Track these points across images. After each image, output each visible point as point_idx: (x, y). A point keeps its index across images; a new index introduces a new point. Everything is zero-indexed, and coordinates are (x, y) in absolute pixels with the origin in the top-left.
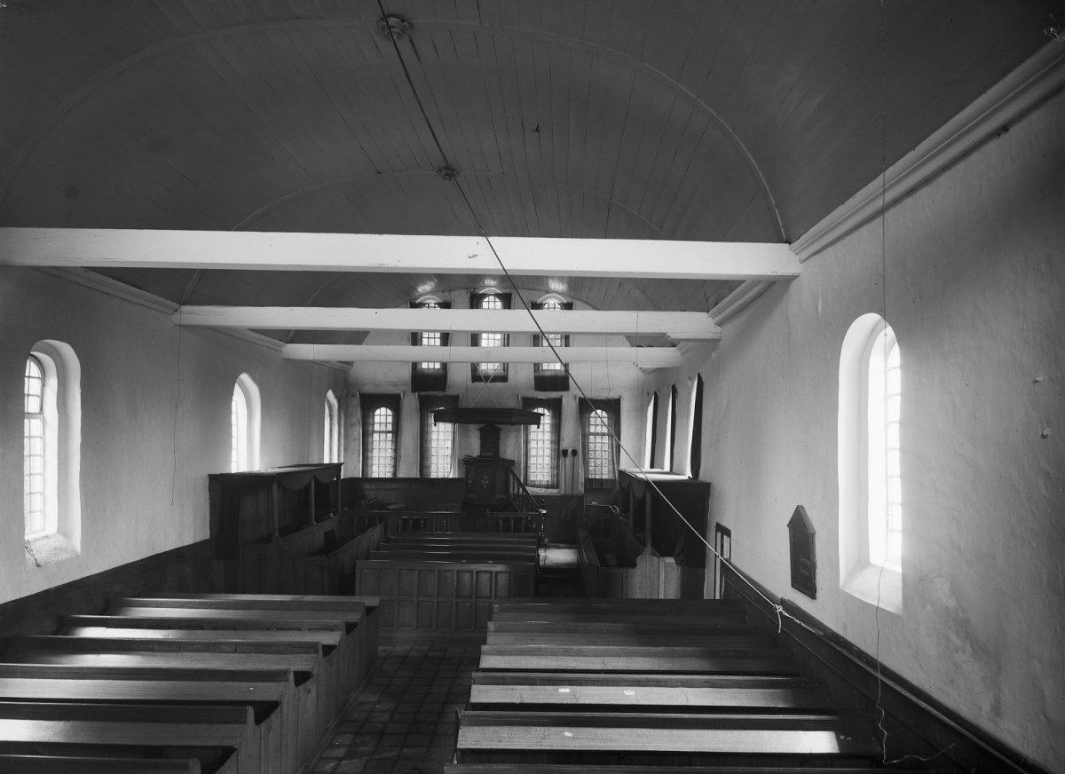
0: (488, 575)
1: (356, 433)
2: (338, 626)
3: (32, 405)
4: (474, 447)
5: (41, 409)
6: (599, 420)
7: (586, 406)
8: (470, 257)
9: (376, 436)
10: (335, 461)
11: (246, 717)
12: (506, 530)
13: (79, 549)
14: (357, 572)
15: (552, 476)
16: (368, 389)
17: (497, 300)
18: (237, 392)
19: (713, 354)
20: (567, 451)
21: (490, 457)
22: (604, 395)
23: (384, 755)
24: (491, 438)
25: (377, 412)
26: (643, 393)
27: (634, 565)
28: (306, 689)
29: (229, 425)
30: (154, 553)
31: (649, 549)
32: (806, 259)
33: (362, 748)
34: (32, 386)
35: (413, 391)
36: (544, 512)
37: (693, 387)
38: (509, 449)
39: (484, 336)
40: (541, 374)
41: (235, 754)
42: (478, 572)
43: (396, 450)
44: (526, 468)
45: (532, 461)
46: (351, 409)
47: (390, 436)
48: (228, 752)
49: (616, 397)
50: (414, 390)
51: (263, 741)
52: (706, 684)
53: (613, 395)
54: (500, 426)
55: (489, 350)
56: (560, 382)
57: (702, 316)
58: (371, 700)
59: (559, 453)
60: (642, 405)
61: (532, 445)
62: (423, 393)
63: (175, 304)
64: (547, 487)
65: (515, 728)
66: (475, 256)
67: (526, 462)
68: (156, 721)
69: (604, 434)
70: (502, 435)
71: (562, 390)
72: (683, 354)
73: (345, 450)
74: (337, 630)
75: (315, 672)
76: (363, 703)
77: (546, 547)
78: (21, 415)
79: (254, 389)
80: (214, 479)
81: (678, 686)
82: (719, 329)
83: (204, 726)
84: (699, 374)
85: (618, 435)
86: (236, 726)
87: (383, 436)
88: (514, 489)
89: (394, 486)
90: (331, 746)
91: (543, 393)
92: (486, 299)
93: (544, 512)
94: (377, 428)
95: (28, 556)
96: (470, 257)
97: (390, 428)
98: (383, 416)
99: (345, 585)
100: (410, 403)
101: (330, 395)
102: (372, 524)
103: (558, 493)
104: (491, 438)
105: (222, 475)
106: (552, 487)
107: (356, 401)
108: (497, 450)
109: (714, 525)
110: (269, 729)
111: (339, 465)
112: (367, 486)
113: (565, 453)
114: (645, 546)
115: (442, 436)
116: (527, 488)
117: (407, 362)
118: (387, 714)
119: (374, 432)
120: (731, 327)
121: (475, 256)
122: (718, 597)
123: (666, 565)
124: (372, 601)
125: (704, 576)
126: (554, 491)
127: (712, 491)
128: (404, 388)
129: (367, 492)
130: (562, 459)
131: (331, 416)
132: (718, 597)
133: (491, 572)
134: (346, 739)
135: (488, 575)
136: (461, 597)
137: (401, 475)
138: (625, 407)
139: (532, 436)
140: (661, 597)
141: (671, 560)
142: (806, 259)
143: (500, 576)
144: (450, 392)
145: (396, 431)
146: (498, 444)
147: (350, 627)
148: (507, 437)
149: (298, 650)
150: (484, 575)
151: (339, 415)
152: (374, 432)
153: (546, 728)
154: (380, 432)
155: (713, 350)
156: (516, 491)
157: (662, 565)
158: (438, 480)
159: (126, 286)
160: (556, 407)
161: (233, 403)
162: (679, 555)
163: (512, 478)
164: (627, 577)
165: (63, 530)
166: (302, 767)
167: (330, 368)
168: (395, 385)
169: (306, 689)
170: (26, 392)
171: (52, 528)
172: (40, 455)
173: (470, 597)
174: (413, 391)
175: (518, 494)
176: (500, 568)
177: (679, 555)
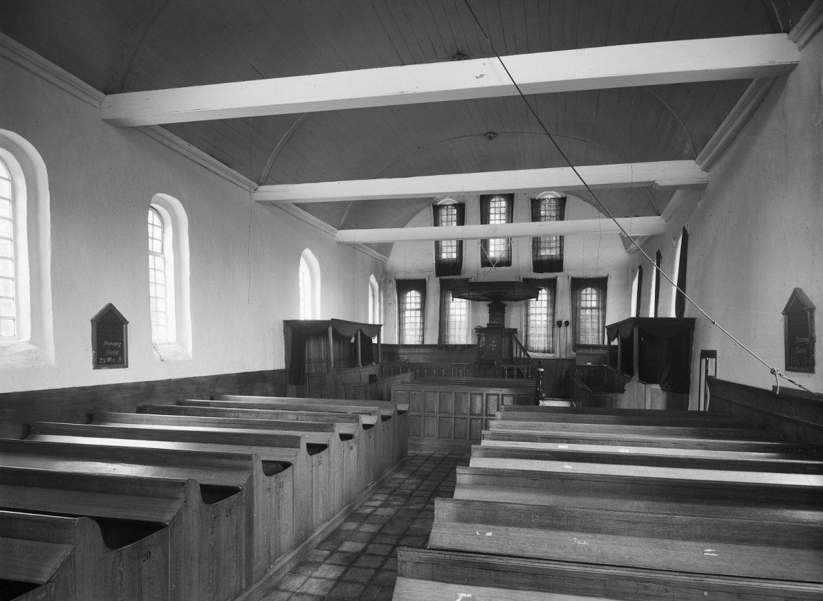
0: (496, 397)
1: (392, 311)
2: (375, 411)
3: (154, 246)
4: (484, 319)
5: (162, 251)
6: (590, 297)
7: (578, 284)
8: (477, 77)
9: (407, 314)
10: (377, 323)
11: (299, 443)
12: (511, 376)
13: (191, 355)
14: (393, 393)
15: (548, 343)
16: (401, 276)
17: (502, 199)
18: (302, 260)
19: (699, 204)
20: (561, 322)
21: (497, 325)
22: (592, 275)
23: (412, 507)
24: (497, 310)
25: (408, 294)
26: (628, 270)
27: (622, 391)
28: (349, 444)
29: (298, 288)
30: (244, 371)
31: (636, 377)
32: (806, 43)
33: (395, 503)
34: (154, 231)
35: (437, 277)
36: (542, 370)
37: (677, 245)
38: (513, 319)
39: (492, 241)
40: (539, 258)
41: (291, 467)
42: (487, 395)
43: (423, 323)
44: (527, 336)
45: (531, 331)
46: (388, 291)
47: (419, 312)
48: (286, 465)
49: (604, 275)
50: (437, 275)
51: (314, 468)
52: (698, 446)
53: (601, 274)
54: (505, 302)
55: (496, 227)
56: (556, 265)
57: (690, 164)
58: (402, 477)
59: (556, 324)
60: (628, 282)
61: (532, 318)
62: (444, 277)
63: (253, 183)
64: (544, 352)
65: (520, 460)
66: (482, 76)
67: (527, 331)
68: (234, 444)
69: (592, 308)
70: (507, 309)
71: (558, 272)
72: (666, 221)
73: (385, 313)
74: (374, 414)
75: (356, 435)
76: (395, 479)
77: (543, 399)
78: (145, 252)
79: (315, 263)
80: (287, 323)
81: (671, 448)
82: (705, 174)
83: (269, 448)
84: (684, 228)
85: (604, 308)
86: (293, 449)
87: (413, 313)
88: (517, 353)
89: (422, 351)
90: (370, 500)
91: (541, 274)
92: (494, 200)
93: (542, 370)
94: (408, 306)
95: (154, 352)
96: (477, 77)
97: (418, 306)
98: (413, 297)
99: (381, 396)
100: (434, 286)
101: (373, 279)
102: (405, 371)
103: (554, 356)
104: (497, 310)
105: (292, 321)
106: (549, 352)
107: (393, 286)
108: (503, 321)
109: (699, 353)
110: (320, 463)
111: (380, 326)
112: (401, 351)
113: (560, 324)
114: (632, 375)
115: (459, 309)
116: (529, 353)
117: (431, 240)
118: (414, 486)
119: (406, 310)
120: (717, 168)
121: (482, 76)
122: (702, 409)
123: (653, 392)
124: (403, 407)
125: (688, 401)
126: (550, 356)
127: (697, 326)
128: (429, 274)
129: (401, 356)
130: (557, 329)
131: (373, 296)
132: (702, 409)
133: (498, 395)
134: (383, 497)
135: (496, 397)
136: (473, 415)
137: (427, 343)
138: (611, 284)
139: (532, 311)
140: (648, 407)
141: (657, 387)
142: (806, 43)
143: (505, 398)
144: (464, 276)
145: (423, 309)
146: (504, 317)
147: (385, 418)
148: (511, 311)
149: (343, 419)
150: (492, 397)
151: (380, 295)
152: (406, 310)
153: (547, 462)
154: (411, 310)
155: (699, 200)
156: (518, 355)
157: (648, 391)
158: (456, 346)
159: (219, 163)
160: (551, 285)
161: (300, 273)
162: (665, 382)
163: (515, 342)
164: (616, 401)
165: (180, 340)
166: (347, 506)
167: (372, 257)
168: (422, 271)
169: (349, 444)
170: (150, 235)
171: (172, 338)
172: (163, 285)
173: (481, 415)
174: (437, 277)
175: (520, 358)
176: (504, 391)
177: (665, 382)
